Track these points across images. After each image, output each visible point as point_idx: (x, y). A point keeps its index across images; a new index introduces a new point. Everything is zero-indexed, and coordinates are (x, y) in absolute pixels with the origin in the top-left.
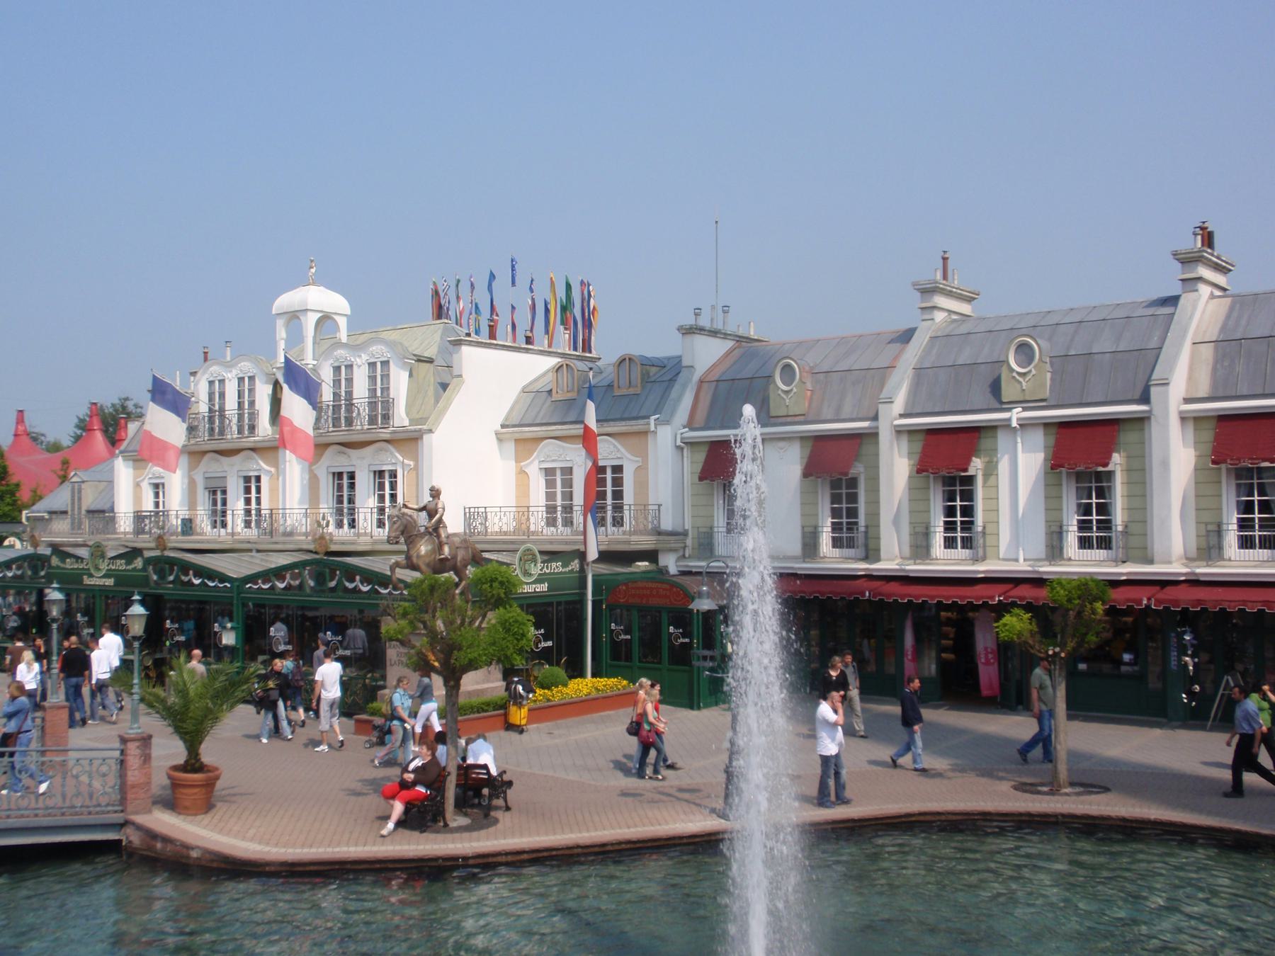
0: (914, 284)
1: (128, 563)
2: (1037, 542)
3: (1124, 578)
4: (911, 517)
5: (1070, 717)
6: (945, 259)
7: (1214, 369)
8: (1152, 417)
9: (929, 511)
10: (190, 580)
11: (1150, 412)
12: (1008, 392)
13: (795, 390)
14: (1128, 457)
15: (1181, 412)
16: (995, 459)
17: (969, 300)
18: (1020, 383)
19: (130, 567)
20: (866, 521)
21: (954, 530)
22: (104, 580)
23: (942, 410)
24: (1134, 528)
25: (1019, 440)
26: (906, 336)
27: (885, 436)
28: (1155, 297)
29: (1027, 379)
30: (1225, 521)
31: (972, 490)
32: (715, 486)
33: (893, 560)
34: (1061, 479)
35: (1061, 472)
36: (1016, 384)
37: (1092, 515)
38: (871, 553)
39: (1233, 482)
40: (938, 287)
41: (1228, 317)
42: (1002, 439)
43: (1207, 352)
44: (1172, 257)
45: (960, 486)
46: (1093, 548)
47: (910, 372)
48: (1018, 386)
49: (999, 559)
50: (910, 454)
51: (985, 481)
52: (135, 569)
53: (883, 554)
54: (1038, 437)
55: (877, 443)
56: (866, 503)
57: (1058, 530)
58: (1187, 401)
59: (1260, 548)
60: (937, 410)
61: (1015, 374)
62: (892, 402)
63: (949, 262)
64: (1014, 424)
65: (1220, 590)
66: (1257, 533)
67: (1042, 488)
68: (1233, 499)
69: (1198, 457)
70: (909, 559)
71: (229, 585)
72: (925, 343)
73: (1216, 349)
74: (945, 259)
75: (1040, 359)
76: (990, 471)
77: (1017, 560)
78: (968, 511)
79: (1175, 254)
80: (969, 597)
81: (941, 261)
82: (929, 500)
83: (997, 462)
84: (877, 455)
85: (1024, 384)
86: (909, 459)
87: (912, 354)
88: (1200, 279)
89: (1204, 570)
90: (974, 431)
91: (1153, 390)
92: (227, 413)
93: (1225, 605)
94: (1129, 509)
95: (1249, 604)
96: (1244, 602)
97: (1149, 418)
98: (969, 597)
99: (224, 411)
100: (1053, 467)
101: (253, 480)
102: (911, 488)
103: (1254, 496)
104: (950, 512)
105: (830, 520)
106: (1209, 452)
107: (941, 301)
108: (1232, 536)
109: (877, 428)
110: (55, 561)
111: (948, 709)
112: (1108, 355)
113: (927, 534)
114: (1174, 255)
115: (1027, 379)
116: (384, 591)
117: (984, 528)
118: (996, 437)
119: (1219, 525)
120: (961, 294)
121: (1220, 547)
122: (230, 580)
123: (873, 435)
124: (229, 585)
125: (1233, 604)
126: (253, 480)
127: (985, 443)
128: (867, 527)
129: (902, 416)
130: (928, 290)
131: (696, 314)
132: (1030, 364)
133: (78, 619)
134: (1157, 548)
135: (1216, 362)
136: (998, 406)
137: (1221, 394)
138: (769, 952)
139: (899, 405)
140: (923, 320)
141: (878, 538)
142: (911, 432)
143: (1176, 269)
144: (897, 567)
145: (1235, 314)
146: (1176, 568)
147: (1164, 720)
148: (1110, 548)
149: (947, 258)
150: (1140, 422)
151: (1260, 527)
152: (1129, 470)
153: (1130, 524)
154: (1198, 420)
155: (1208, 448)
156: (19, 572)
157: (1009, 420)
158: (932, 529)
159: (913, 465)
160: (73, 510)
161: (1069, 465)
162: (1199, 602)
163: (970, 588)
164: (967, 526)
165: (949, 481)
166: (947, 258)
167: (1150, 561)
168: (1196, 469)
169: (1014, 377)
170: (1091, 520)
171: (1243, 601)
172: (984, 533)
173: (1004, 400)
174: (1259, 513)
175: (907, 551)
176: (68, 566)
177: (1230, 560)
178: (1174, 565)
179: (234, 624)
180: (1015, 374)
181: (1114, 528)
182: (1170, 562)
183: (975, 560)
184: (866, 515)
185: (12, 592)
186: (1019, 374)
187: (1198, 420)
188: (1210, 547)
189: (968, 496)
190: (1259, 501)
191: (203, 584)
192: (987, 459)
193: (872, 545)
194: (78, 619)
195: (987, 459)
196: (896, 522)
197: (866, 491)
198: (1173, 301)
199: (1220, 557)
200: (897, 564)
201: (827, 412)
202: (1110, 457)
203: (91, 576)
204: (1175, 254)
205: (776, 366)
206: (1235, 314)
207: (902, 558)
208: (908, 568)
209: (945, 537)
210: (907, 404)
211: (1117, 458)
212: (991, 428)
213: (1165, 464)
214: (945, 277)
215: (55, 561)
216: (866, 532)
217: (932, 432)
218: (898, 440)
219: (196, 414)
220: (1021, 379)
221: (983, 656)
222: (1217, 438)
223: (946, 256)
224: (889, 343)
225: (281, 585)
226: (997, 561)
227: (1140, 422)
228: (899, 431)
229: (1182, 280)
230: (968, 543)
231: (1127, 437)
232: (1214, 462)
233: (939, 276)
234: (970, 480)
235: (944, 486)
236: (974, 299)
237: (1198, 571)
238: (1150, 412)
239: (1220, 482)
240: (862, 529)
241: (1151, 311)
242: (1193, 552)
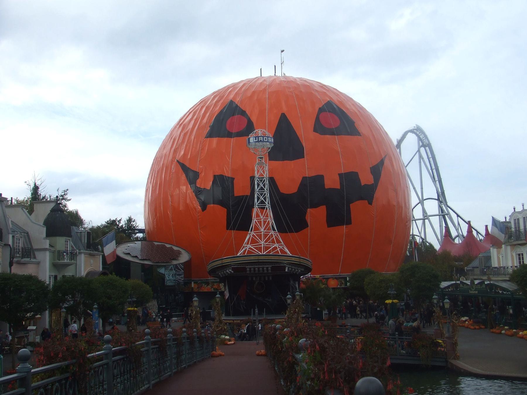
1: (481, 286)
6: (523, 205)
10: (499, 291)
19: (481, 287)
22: (475, 291)
52: (483, 288)
71: (510, 293)
74: (523, 205)
81: (522, 206)
92: (521, 230)
99: (520, 230)
101: (521, 255)
110: (461, 286)
116: (505, 293)
122: (510, 291)
124: (510, 293)
126: (521, 255)
133: (494, 307)
138: (526, 384)
156: (452, 289)
160: (480, 267)
176: (465, 287)
179: (512, 307)
185: (326, 286)
191: (502, 293)
194: (459, 304)
203: (471, 290)
215: (461, 286)
219: (511, 231)
225: (450, 290)
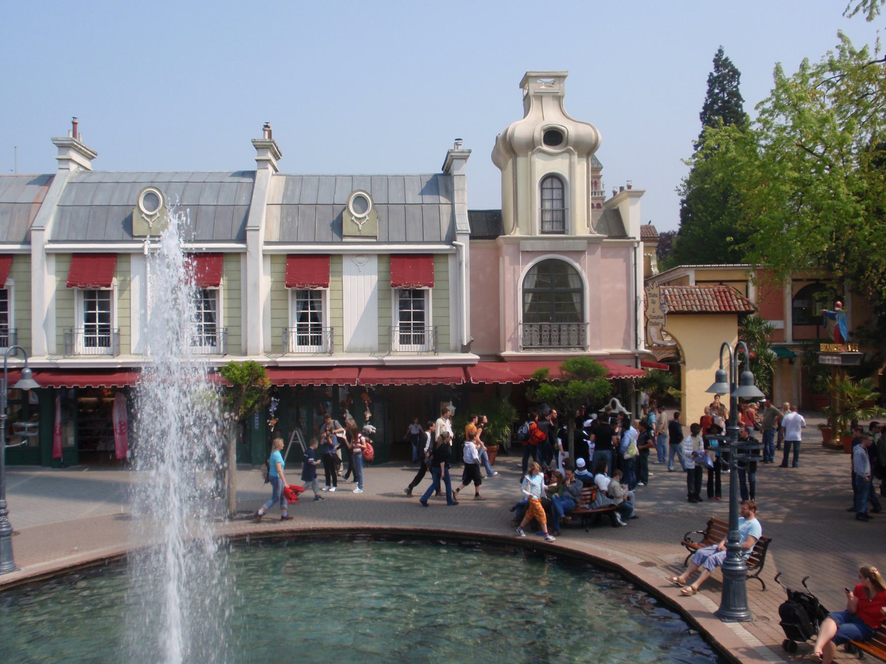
0: (53, 140)
2: (372, 339)
3: (119, 366)
4: (57, 322)
5: (240, 468)
6: (74, 124)
7: (282, 224)
8: (248, 253)
9: (73, 317)
11: (246, 249)
12: (138, 229)
13: (158, 215)
14: (229, 280)
15: (263, 251)
16: (128, 279)
17: (90, 158)
18: (148, 222)
20: (16, 323)
21: (94, 331)
23: (84, 239)
24: (232, 331)
25: (148, 265)
26: (47, 180)
27: (37, 258)
28: (235, 171)
29: (153, 220)
30: (290, 326)
31: (109, 302)
32: (76, 292)
33: (43, 356)
34: (73, 295)
35: (73, 290)
36: (144, 223)
37: (95, 322)
38: (26, 352)
39: (295, 300)
40: (73, 144)
41: (286, 188)
42: (135, 263)
43: (277, 210)
44: (51, 142)
45: (99, 298)
46: (410, 343)
47: (55, 208)
48: (146, 225)
49: (131, 354)
50: (58, 272)
51: (121, 294)
53: (34, 352)
54: (374, 263)
55: (30, 263)
56: (15, 310)
57: (69, 332)
58: (267, 243)
59: (312, 344)
60: (79, 238)
61: (143, 216)
62: (44, 230)
63: (78, 126)
64: (146, 252)
65: (293, 372)
66: (310, 335)
67: (376, 300)
68: (295, 312)
69: (273, 282)
70: (56, 354)
72: (64, 187)
73: (282, 209)
74: (74, 124)
75: (164, 206)
76: (125, 287)
77: (146, 354)
78: (105, 318)
79: (254, 142)
80: (114, 383)
82: (74, 308)
83: (130, 281)
84: (29, 272)
85: (151, 223)
86: (57, 276)
87: (56, 192)
88: (70, 160)
89: (64, 361)
90: (112, 256)
91: (248, 233)
93: (300, 382)
94: (229, 317)
95: (316, 381)
96: (312, 380)
97: (245, 253)
98: (114, 383)
100: (69, 286)
102: (58, 299)
103: (95, 310)
104: (90, 318)
105: (84, 324)
106: (66, 279)
107: (73, 155)
108: (81, 337)
109: (30, 250)
111: (88, 470)
112: (211, 207)
113: (389, 335)
114: (253, 142)
115: (153, 220)
117: (119, 330)
118: (130, 262)
119: (286, 329)
120: (86, 153)
121: (72, 345)
123: (27, 256)
125: (305, 381)
127: (120, 266)
128: (16, 330)
129: (51, 242)
130: (63, 146)
131: (456, 144)
132: (155, 208)
134: (250, 344)
135: (282, 218)
136: (131, 239)
137: (287, 240)
139: (47, 234)
140: (60, 169)
141: (30, 339)
142: (59, 255)
143: (254, 154)
144: (48, 361)
145: (290, 188)
146: (262, 358)
147: (249, 465)
148: (109, 346)
149: (76, 123)
150: (238, 255)
151: (100, 331)
152: (229, 290)
153: (229, 328)
154: (273, 257)
155: (65, 276)
157: (143, 249)
158: (76, 331)
159: (60, 281)
161: (81, 284)
162: (283, 381)
163: (111, 376)
164: (105, 329)
165: (90, 294)
166: (76, 123)
167: (245, 354)
168: (57, 290)
169: (143, 218)
170: (308, 325)
171: (392, 378)
172: (118, 334)
173: (135, 235)
174: (99, 322)
175: (54, 348)
177: (293, 352)
178: (261, 356)
180: (143, 216)
181: (111, 331)
182: (258, 354)
183: (112, 355)
184: (16, 320)
186: (147, 215)
187: (273, 257)
188: (281, 346)
189: (106, 306)
190: (99, 313)
192: (122, 278)
193: (581, 338)
195: (122, 278)
196: (46, 325)
197: (16, 301)
198: (252, 174)
199: (390, 350)
200: (47, 359)
201: (394, 237)
202: (111, 280)
204: (254, 142)
205: (141, 191)
206: (290, 188)
207: (49, 354)
208: (58, 361)
209: (400, 335)
210: (53, 234)
211: (223, 282)
212: (126, 255)
213: (256, 286)
214: (74, 135)
216: (16, 334)
217: (77, 256)
218: (47, 259)
220: (148, 220)
221: (118, 428)
222: (288, 269)
223: (76, 121)
224: (28, 184)
226: (129, 356)
227: (238, 255)
228: (49, 254)
229: (257, 160)
230: (105, 342)
231: (228, 266)
232: (288, 286)
233: (71, 136)
234: (108, 294)
235: (85, 298)
236: (94, 157)
237: (278, 360)
238: (246, 249)
239: (287, 300)
240: (12, 331)
241: (236, 179)
242: (269, 348)
